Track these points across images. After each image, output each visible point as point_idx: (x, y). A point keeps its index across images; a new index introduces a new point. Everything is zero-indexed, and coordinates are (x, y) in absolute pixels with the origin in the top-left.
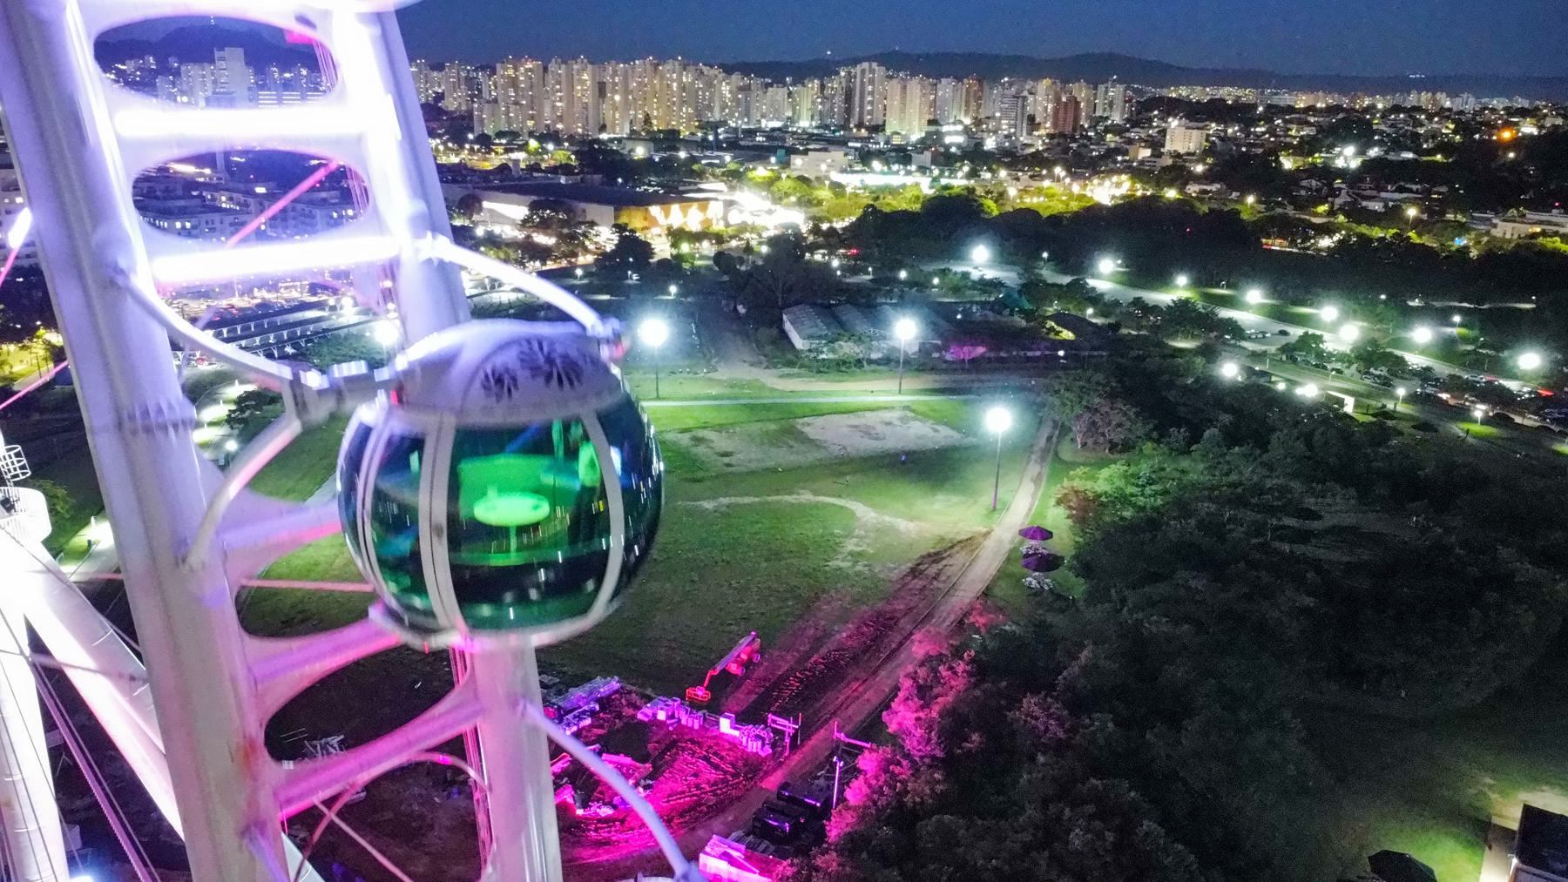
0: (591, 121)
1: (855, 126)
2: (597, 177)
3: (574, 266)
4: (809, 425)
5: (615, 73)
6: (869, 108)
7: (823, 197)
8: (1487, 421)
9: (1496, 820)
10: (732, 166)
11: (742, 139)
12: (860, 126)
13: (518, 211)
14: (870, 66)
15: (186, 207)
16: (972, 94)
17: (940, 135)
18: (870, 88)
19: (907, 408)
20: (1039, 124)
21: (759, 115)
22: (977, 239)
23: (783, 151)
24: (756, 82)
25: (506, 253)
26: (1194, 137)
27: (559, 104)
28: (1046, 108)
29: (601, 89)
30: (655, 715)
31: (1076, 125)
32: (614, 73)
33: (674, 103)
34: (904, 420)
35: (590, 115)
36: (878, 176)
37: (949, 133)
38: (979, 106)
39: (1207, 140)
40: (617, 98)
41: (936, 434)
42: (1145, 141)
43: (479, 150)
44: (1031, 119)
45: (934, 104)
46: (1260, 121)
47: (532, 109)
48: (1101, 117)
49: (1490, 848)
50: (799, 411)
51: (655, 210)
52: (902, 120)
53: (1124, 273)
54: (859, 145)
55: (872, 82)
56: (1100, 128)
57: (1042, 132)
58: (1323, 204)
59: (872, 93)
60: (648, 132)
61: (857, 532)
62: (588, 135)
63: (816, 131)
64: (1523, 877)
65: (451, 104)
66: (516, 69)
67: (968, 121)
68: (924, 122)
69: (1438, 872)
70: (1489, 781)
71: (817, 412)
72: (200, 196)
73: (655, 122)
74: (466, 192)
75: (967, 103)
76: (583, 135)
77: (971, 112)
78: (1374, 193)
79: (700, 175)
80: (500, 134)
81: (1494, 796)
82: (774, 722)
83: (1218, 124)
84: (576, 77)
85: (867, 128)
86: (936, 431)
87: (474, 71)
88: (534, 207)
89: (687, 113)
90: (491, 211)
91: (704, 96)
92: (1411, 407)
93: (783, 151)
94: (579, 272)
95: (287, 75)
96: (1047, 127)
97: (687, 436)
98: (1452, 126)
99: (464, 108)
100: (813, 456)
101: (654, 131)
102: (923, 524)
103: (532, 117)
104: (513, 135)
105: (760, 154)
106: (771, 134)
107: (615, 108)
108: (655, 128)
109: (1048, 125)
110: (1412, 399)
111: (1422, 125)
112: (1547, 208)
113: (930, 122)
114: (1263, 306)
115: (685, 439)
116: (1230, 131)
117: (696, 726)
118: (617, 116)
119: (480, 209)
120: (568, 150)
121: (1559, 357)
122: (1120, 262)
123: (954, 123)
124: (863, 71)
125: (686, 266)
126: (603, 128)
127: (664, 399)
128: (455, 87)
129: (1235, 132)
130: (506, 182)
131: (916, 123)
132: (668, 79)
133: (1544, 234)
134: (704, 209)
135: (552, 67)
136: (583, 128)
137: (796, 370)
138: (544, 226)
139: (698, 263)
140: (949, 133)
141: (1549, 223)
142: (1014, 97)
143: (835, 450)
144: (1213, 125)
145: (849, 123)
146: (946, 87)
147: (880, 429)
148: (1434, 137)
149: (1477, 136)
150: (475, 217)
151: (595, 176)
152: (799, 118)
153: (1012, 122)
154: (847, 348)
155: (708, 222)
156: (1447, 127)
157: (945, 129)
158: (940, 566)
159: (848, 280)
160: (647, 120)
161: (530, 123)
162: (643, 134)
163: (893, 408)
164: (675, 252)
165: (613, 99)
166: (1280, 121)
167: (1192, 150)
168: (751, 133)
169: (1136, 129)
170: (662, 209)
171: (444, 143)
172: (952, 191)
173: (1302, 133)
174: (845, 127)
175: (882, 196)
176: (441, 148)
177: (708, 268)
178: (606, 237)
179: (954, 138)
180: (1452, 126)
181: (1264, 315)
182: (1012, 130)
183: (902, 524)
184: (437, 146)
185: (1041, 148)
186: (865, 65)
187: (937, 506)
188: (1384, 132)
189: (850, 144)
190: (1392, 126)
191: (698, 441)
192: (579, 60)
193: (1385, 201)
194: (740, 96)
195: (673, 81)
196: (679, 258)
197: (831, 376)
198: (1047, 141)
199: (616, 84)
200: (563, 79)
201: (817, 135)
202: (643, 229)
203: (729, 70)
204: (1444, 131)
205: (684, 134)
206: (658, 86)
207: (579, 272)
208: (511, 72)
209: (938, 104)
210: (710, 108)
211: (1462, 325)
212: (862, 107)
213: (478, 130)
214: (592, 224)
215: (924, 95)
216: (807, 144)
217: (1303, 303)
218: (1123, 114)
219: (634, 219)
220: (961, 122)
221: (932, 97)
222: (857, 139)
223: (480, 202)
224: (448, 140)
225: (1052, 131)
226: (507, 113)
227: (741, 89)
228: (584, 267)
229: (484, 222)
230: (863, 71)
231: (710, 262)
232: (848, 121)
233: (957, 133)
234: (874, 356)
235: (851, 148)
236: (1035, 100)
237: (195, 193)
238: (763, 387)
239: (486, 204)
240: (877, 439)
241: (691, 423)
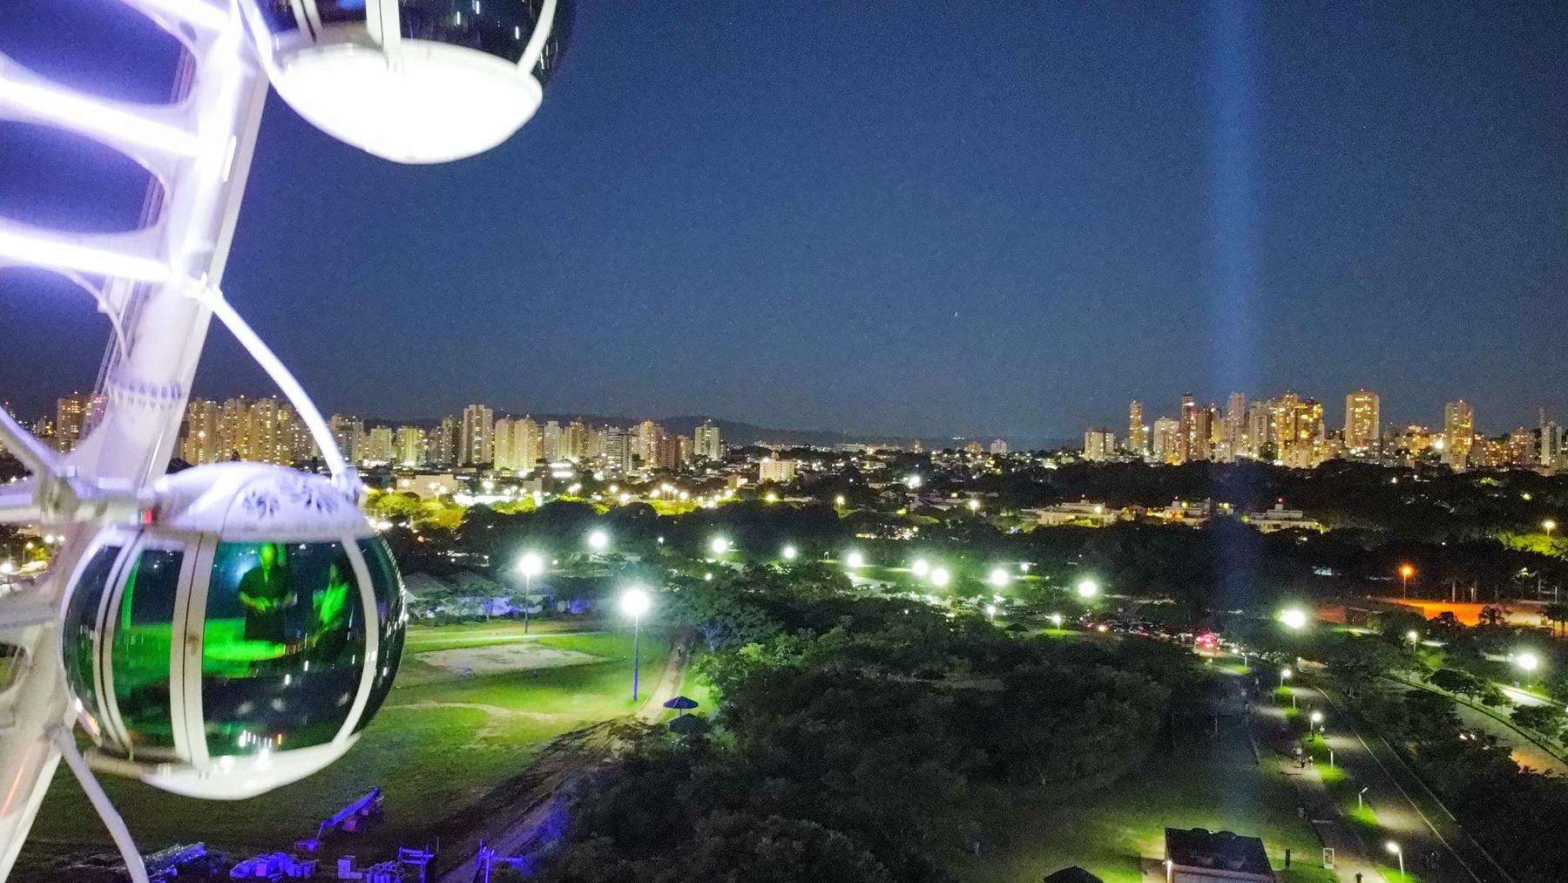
6: (477, 447)
8: (1064, 627)
9: (1144, 855)
14: (477, 408)
16: (578, 435)
18: (477, 429)
20: (644, 461)
26: (784, 468)
28: (649, 445)
31: (678, 461)
33: (267, 441)
37: (559, 470)
38: (585, 447)
39: (796, 473)
40: (202, 434)
41: (568, 657)
42: (741, 474)
44: (636, 458)
45: (541, 445)
46: (839, 458)
48: (700, 455)
49: (1146, 873)
52: (510, 458)
53: (736, 552)
54: (468, 478)
55: (479, 423)
56: (700, 463)
57: (647, 467)
58: (901, 509)
59: (479, 434)
61: (490, 724)
64: (1181, 879)
66: (82, 405)
67: (576, 460)
69: (1105, 882)
70: (1130, 831)
75: (574, 445)
77: (578, 452)
78: (940, 499)
81: (1138, 841)
83: (804, 461)
92: (1002, 623)
96: (652, 463)
98: (993, 462)
107: (199, 445)
109: (652, 461)
111: (969, 461)
112: (1076, 499)
113: (538, 461)
114: (860, 569)
116: (814, 465)
121: (1110, 585)
122: (731, 543)
123: (562, 461)
124: (471, 413)
129: (819, 467)
131: (524, 460)
133: (1077, 518)
140: (559, 470)
141: (1080, 512)
144: (799, 461)
147: (507, 656)
148: (980, 471)
149: (1013, 470)
152: (404, 457)
153: (619, 458)
156: (989, 463)
157: (553, 465)
158: (584, 740)
165: (196, 436)
166: (855, 459)
167: (783, 479)
169: (733, 465)
173: (874, 468)
180: (993, 462)
181: (866, 577)
182: (619, 465)
183: (539, 716)
185: (646, 481)
187: (575, 702)
188: (941, 466)
190: (946, 461)
193: (951, 505)
194: (341, 435)
195: (267, 419)
198: (653, 474)
199: (202, 421)
204: (987, 465)
208: (76, 409)
209: (546, 444)
211: (1030, 573)
212: (470, 439)
215: (531, 434)
217: (896, 565)
218: (718, 454)
221: (540, 439)
225: (656, 467)
227: (343, 429)
230: (471, 413)
232: (455, 461)
233: (565, 469)
234: (496, 612)
236: (638, 442)
240: (505, 663)
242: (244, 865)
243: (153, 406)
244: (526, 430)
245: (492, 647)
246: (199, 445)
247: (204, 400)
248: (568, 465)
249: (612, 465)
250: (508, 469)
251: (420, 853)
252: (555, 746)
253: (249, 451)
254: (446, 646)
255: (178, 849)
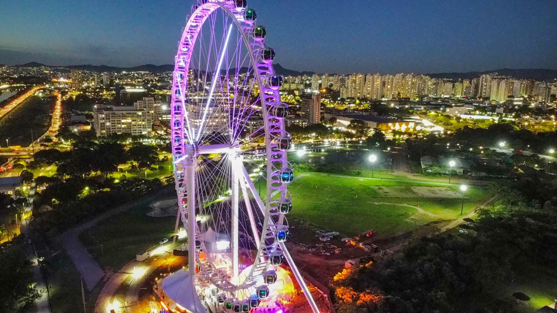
0: (379, 94)
1: (479, 97)
2: (376, 113)
3: (359, 141)
4: (415, 188)
5: (389, 79)
7: (453, 123)
10: (424, 111)
11: (432, 101)
12: (480, 98)
13: (347, 123)
14: (486, 76)
15: (255, 118)
17: (512, 101)
19: (450, 187)
21: (441, 93)
22: (500, 140)
23: (444, 106)
24: (440, 81)
25: (340, 135)
27: (369, 89)
29: (384, 84)
30: (345, 241)
32: (388, 78)
33: (409, 89)
34: (446, 190)
35: (379, 92)
36: (477, 116)
37: (517, 101)
38: (532, 91)
40: (389, 87)
43: (340, 103)
47: (360, 90)
50: (413, 184)
51: (390, 124)
60: (399, 98)
62: (377, 99)
63: (462, 99)
65: (334, 88)
66: (356, 77)
68: (506, 96)
71: (419, 185)
72: (258, 115)
73: (402, 95)
74: (332, 117)
75: (526, 90)
76: (375, 99)
79: (412, 114)
80: (348, 98)
82: (373, 245)
84: (375, 80)
85: (483, 98)
86: (456, 194)
87: (345, 76)
88: (352, 122)
89: (413, 92)
90: (339, 123)
91: (422, 86)
93: (444, 106)
94: (361, 142)
95: (286, 78)
97: (377, 187)
99: (338, 89)
100: (413, 196)
101: (401, 98)
102: (436, 215)
103: (359, 93)
104: (353, 98)
105: (436, 107)
106: (444, 100)
107: (388, 90)
108: (402, 97)
110: (350, 147)
113: (509, 97)
115: (376, 188)
117: (354, 244)
118: (388, 93)
119: (336, 122)
120: (369, 104)
124: (483, 78)
125: (397, 142)
126: (383, 97)
127: (375, 178)
128: (337, 82)
130: (345, 114)
131: (502, 97)
132: (408, 81)
134: (407, 125)
135: (368, 77)
136: (376, 96)
137: (419, 174)
138: (354, 128)
139: (401, 142)
142: (545, 88)
143: (420, 195)
145: (476, 96)
146: (517, 83)
147: (437, 191)
150: (334, 124)
151: (375, 113)
154: (436, 169)
155: (409, 129)
159: (451, 150)
160: (399, 94)
161: (359, 95)
162: (397, 99)
163: (445, 187)
164: (394, 138)
165: (387, 86)
168: (437, 99)
170: (392, 124)
171: (330, 101)
172: (506, 122)
174: (474, 97)
175: (477, 123)
176: (328, 102)
177: (404, 143)
178: (371, 132)
179: (518, 102)
182: (544, 100)
184: (327, 102)
186: (484, 76)
189: (474, 104)
191: (380, 189)
192: (377, 75)
196: (395, 140)
197: (430, 177)
199: (389, 82)
200: (371, 81)
201: (462, 100)
202: (385, 130)
203: (432, 76)
205: (412, 99)
206: (404, 83)
207: (361, 142)
208: (354, 78)
209: (514, 90)
210: (424, 90)
212: (482, 87)
213: (341, 97)
214: (369, 128)
216: (457, 104)
219: (383, 127)
220: (523, 97)
222: (478, 102)
223: (336, 119)
224: (331, 100)
226: (351, 91)
228: (363, 141)
229: (336, 126)
231: (405, 142)
232: (475, 95)
233: (520, 101)
235: (474, 105)
237: (257, 114)
238: (407, 178)
239: (338, 120)
241: (380, 184)
242: (344, 239)
243: (284, 229)
244: (504, 85)
245: (435, 187)
246: (388, 90)
247: (390, 75)
248: (522, 99)
249: (540, 100)
250: (495, 101)
251: (375, 246)
252: (427, 225)
253: (403, 91)
254: (423, 185)
255: (334, 233)
